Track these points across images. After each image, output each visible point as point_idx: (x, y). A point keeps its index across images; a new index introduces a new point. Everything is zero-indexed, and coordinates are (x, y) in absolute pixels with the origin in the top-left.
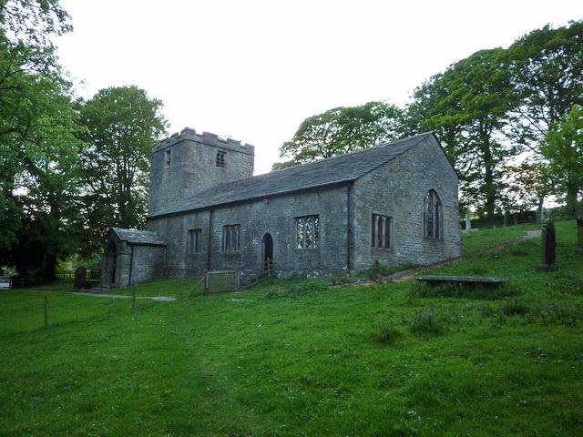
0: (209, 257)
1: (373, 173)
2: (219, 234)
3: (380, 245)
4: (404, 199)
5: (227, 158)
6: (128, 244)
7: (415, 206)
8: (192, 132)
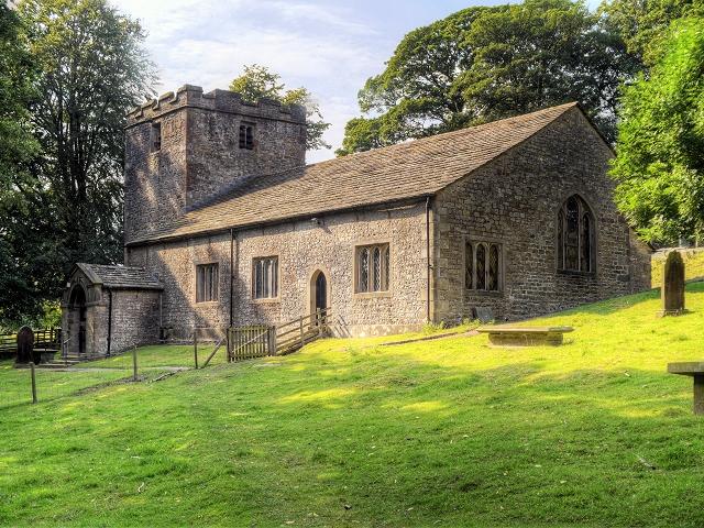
2: (246, 273)
3: (481, 285)
4: (522, 215)
5: (258, 134)
6: (104, 288)
8: (198, 91)
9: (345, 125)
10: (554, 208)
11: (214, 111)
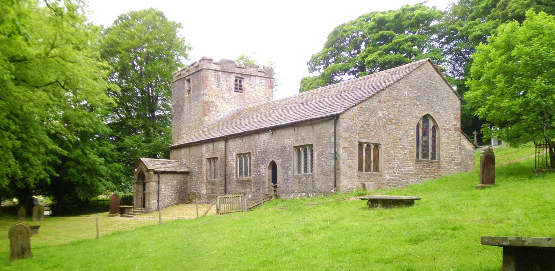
0: (226, 182)
1: (359, 106)
2: (233, 162)
3: (368, 169)
4: (394, 127)
5: (245, 83)
6: (156, 172)
7: (407, 131)
9: (300, 80)
10: (414, 122)
11: (219, 71)
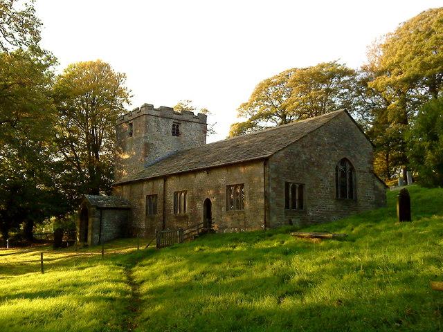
1: (285, 150)
4: (316, 169)
5: (182, 128)
6: (98, 208)
8: (151, 107)
